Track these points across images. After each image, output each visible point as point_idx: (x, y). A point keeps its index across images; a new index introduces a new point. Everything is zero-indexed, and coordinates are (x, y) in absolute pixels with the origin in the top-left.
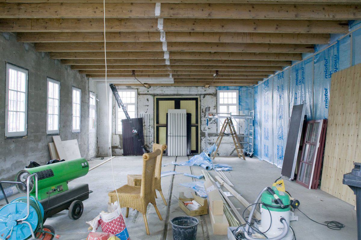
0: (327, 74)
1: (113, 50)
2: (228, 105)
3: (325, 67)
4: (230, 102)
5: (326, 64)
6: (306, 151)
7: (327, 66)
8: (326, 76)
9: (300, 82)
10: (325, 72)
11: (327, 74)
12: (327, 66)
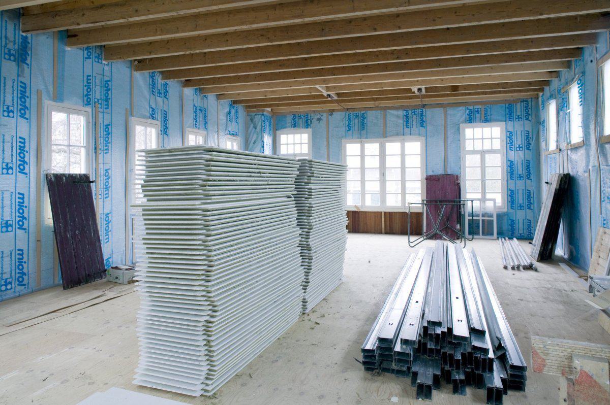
2: (483, 153)
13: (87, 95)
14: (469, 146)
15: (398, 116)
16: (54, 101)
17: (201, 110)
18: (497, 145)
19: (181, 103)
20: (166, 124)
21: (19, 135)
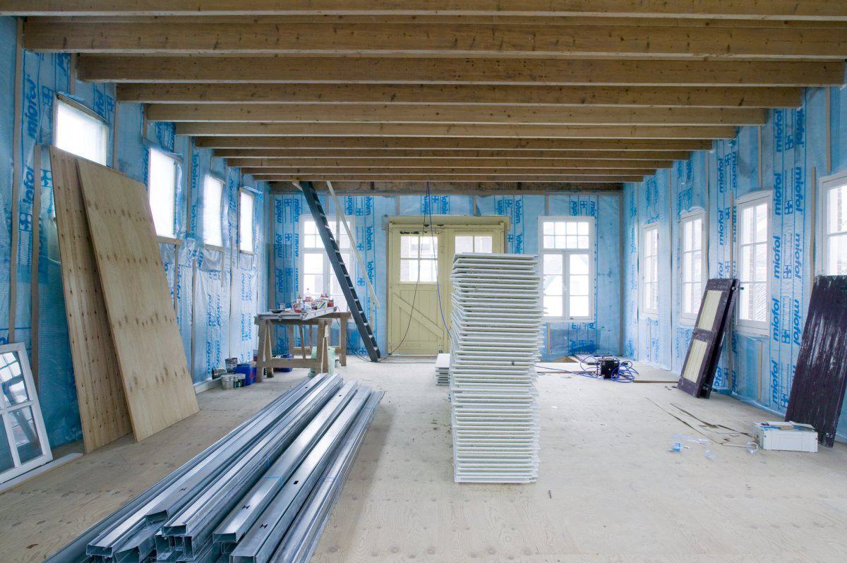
0: (780, 143)
1: (217, 100)
2: (566, 253)
3: (772, 378)
4: (571, 246)
5: (778, 184)
6: (254, 435)
7: (779, 188)
8: (779, 146)
9: (727, 161)
10: (775, 264)
11: (780, 143)
12: (779, 188)
13: (372, 269)
14: (547, 243)
15: (564, 201)
16: (81, 80)
17: (788, 272)
18: (585, 243)
19: (759, 200)
20: (774, 380)
21: (801, 279)
